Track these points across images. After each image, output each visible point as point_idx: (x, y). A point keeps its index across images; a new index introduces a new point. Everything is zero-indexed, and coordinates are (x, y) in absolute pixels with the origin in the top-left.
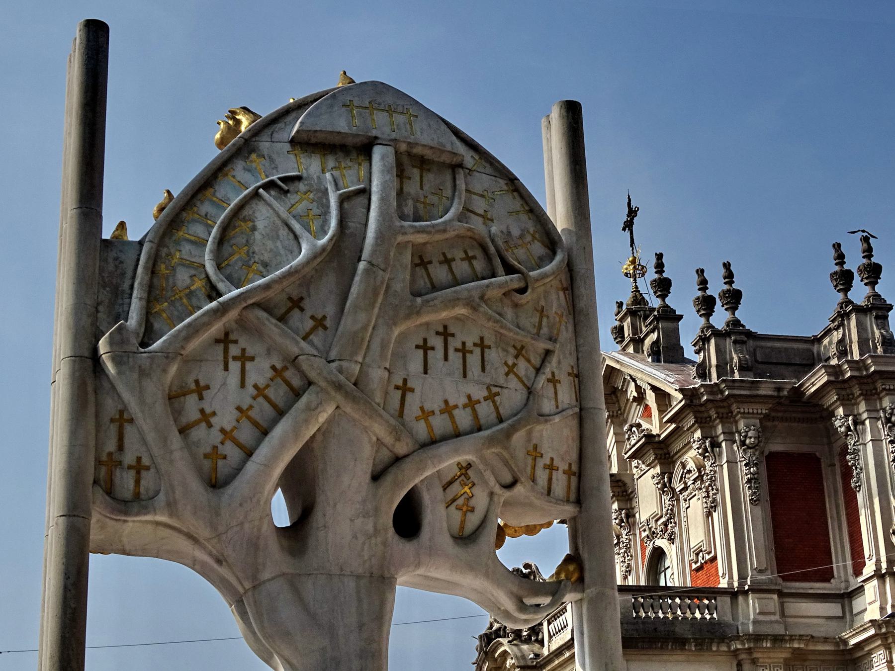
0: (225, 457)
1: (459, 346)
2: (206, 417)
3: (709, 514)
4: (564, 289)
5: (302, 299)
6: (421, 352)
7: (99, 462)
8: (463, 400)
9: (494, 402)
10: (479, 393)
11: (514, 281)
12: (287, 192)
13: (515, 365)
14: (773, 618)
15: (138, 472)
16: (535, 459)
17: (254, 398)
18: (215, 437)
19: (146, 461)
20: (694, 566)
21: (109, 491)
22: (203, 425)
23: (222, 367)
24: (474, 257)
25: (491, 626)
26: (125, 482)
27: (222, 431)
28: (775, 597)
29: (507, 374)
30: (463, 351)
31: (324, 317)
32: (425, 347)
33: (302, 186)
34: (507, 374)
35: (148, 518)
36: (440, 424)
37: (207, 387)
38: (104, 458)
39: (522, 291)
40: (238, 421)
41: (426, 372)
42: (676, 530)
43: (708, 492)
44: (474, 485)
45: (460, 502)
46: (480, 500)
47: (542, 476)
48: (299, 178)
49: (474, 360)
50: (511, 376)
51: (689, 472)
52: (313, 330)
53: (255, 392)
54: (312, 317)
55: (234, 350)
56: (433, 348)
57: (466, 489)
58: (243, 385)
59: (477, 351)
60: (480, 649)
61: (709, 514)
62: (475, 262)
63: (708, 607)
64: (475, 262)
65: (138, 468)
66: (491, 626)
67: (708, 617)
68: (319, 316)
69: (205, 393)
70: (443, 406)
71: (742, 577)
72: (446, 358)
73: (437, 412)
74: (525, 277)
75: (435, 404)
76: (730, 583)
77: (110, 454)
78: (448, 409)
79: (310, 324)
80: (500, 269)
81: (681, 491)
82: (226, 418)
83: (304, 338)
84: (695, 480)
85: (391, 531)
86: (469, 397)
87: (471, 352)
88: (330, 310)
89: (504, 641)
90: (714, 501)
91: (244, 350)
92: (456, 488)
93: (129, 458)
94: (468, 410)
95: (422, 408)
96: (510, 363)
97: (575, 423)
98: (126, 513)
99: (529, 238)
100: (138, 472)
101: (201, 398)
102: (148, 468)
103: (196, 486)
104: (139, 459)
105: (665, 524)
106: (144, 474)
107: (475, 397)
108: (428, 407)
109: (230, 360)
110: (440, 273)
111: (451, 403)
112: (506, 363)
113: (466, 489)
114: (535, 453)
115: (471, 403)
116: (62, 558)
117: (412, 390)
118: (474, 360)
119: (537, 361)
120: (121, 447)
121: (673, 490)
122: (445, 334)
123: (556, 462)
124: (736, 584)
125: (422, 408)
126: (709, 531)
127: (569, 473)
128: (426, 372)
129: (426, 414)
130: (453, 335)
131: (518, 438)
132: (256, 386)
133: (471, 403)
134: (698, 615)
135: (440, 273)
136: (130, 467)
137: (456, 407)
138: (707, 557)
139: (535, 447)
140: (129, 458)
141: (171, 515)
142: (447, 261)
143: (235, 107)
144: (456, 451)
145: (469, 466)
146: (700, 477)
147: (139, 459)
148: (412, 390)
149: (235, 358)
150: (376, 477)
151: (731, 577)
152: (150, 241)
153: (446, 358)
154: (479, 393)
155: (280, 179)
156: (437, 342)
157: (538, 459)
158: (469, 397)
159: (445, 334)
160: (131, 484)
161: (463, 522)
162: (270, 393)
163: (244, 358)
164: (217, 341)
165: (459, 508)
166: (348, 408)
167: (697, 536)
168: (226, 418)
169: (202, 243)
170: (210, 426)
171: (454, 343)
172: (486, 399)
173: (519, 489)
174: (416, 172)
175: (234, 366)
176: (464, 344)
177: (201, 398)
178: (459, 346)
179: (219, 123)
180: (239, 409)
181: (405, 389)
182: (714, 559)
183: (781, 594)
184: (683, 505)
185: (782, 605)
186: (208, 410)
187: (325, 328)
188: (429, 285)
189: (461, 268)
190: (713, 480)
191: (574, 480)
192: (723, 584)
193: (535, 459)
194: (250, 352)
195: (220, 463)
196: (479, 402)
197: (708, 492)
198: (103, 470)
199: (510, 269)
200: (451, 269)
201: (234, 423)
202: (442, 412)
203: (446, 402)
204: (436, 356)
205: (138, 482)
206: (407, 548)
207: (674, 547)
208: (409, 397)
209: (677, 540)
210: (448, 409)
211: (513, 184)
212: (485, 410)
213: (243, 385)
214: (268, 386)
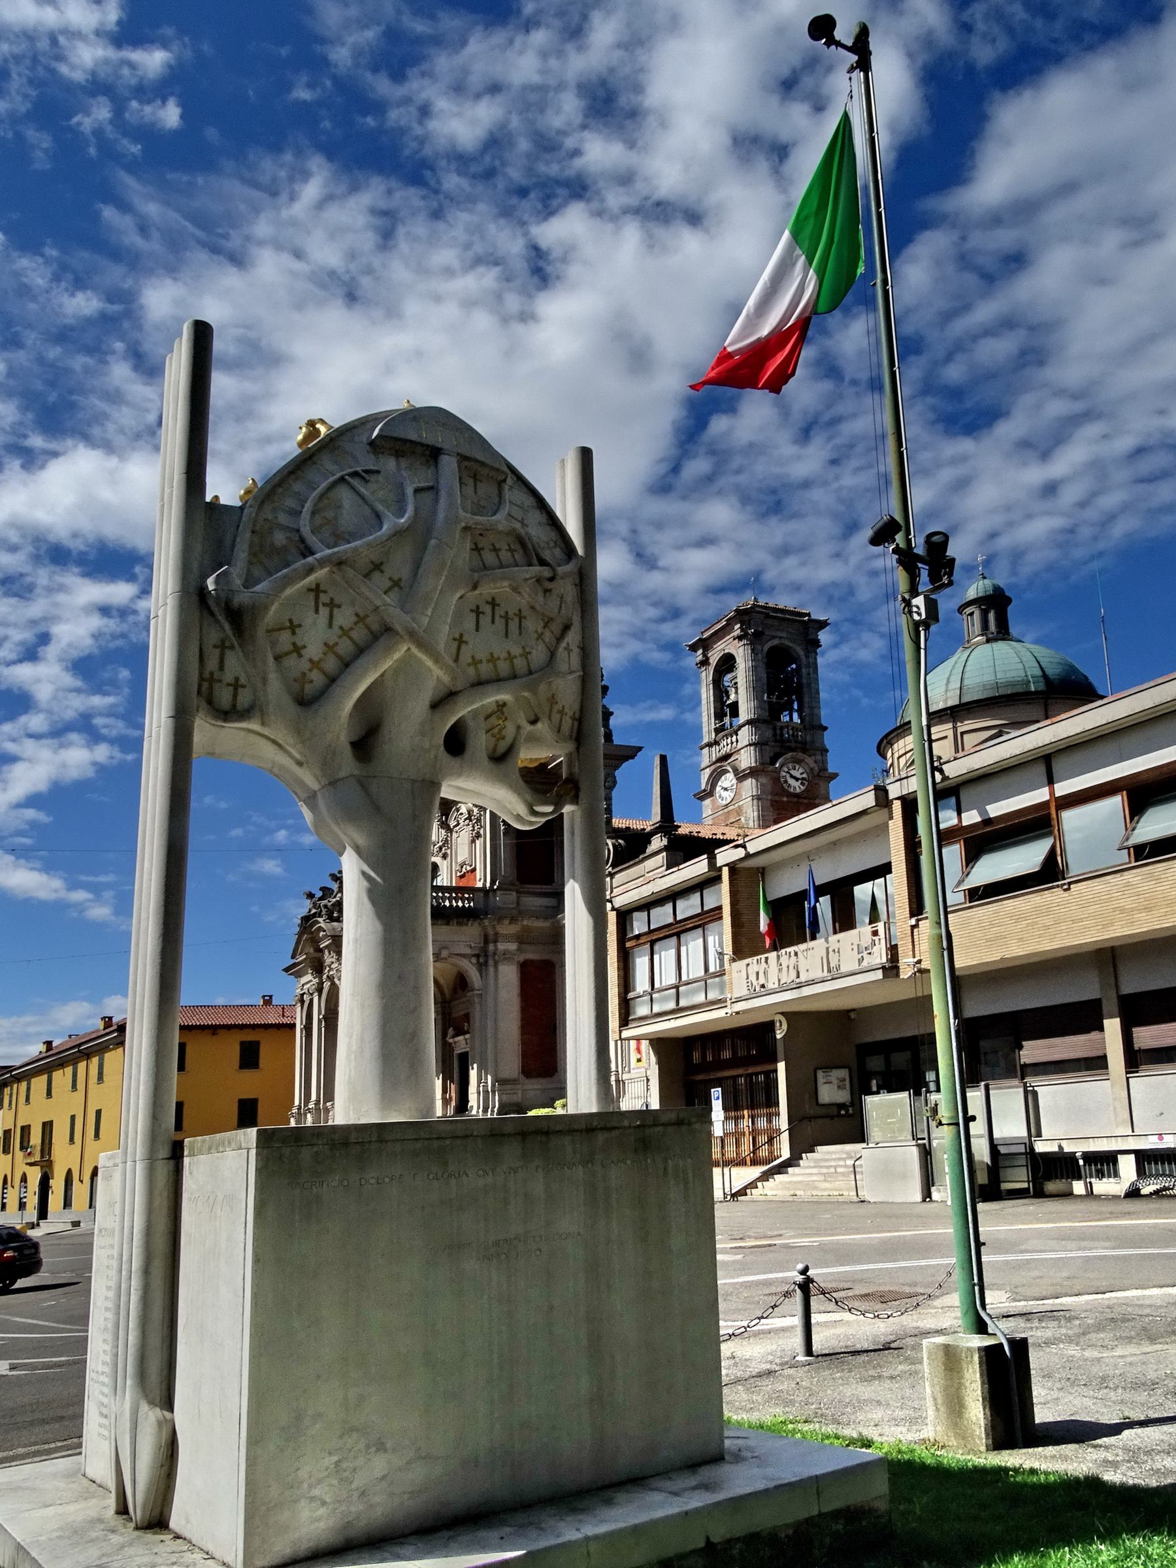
0: (311, 682)
1: (503, 614)
2: (297, 650)
3: (473, 841)
4: (576, 585)
5: (382, 563)
6: (474, 615)
7: (201, 678)
8: (504, 655)
9: (526, 658)
10: (516, 651)
11: (546, 572)
12: (367, 482)
13: (542, 634)
14: (511, 906)
15: (236, 689)
16: (551, 706)
17: (340, 637)
18: (304, 665)
19: (243, 681)
20: (459, 874)
21: (210, 702)
22: (295, 655)
23: (313, 609)
24: (515, 551)
25: (310, 911)
26: (224, 697)
27: (311, 660)
28: (514, 893)
29: (537, 639)
30: (506, 617)
31: (400, 580)
32: (477, 612)
33: (380, 478)
34: (537, 639)
35: (244, 725)
36: (485, 670)
37: (300, 626)
38: (206, 675)
39: (551, 579)
40: (324, 654)
41: (477, 630)
42: (449, 851)
43: (473, 827)
44: (506, 719)
45: (496, 731)
46: (510, 731)
47: (556, 717)
48: (378, 472)
49: (514, 625)
50: (540, 641)
51: (462, 814)
52: (390, 589)
53: (340, 632)
54: (390, 579)
55: (324, 598)
56: (483, 613)
57: (501, 722)
58: (330, 625)
59: (517, 619)
60: (301, 926)
61: (473, 841)
62: (515, 553)
63: (467, 899)
64: (515, 553)
65: (236, 685)
66: (310, 911)
67: (467, 906)
68: (396, 578)
69: (297, 630)
70: (489, 657)
71: (493, 882)
72: (493, 622)
73: (484, 661)
74: (554, 570)
75: (482, 655)
76: (484, 884)
77: (212, 674)
78: (492, 659)
79: (388, 584)
80: (535, 561)
81: (455, 826)
82: (314, 650)
83: (385, 593)
84: (465, 820)
85: (442, 748)
86: (509, 653)
87: (512, 619)
88: (405, 573)
89: (320, 920)
90: (478, 833)
91: (332, 599)
92: (493, 720)
93: (228, 677)
94: (508, 662)
95: (473, 657)
96: (540, 631)
97: (579, 683)
98: (225, 720)
99: (552, 544)
100: (236, 689)
101: (294, 633)
102: (243, 686)
103: (287, 701)
104: (237, 679)
105: (441, 848)
106: (240, 690)
107: (513, 654)
108: (478, 656)
109: (321, 605)
110: (489, 558)
111: (496, 655)
112: (536, 631)
113: (501, 722)
114: (553, 700)
115: (510, 657)
116: (662, 460)
117: (466, 643)
118: (514, 625)
119: (558, 632)
120: (221, 667)
121: (449, 826)
122: (493, 603)
123: (566, 710)
124: (488, 885)
125: (473, 657)
126: (472, 853)
127: (573, 718)
128: (477, 630)
129: (475, 662)
130: (499, 605)
131: (542, 687)
132: (341, 628)
133: (510, 657)
134: (460, 904)
135: (489, 558)
136: (229, 685)
137: (499, 659)
138: (469, 868)
139: (553, 696)
140: (228, 677)
141: (263, 724)
142: (495, 550)
143: (315, 417)
144: (498, 692)
145: (504, 704)
146: (469, 818)
147: (237, 679)
148: (466, 643)
149: (324, 605)
150: (435, 706)
151: (485, 880)
152: (251, 506)
153: (493, 622)
154: (516, 651)
155: (363, 471)
156: (487, 609)
157: (554, 706)
158: (509, 653)
159: (493, 603)
160: (230, 698)
161: (496, 746)
162: (354, 634)
163: (332, 605)
164: (310, 590)
165: (493, 736)
166: (414, 650)
167: (462, 854)
168: (314, 650)
169: (297, 514)
170: (300, 656)
171: (500, 612)
172: (521, 655)
173: (539, 725)
174: (471, 481)
175: (324, 612)
176: (507, 613)
177: (294, 633)
178: (503, 614)
179: (301, 428)
180: (326, 644)
181: (460, 641)
182: (474, 870)
183: (518, 892)
184: (455, 835)
185: (518, 898)
186: (300, 644)
187: (401, 588)
188: (481, 565)
189: (505, 555)
190: (479, 820)
191: (576, 723)
192: (479, 885)
193: (551, 706)
194: (337, 601)
195: (307, 686)
196: (516, 657)
197: (473, 827)
198: (205, 685)
199: (542, 562)
200: (498, 555)
201: (321, 655)
202: (489, 661)
203: (492, 654)
204: (485, 620)
205: (235, 696)
206: (454, 762)
207: (445, 862)
208: (464, 647)
209: (449, 859)
210: (492, 659)
211: (541, 504)
212: (520, 663)
213: (330, 625)
214: (351, 629)
